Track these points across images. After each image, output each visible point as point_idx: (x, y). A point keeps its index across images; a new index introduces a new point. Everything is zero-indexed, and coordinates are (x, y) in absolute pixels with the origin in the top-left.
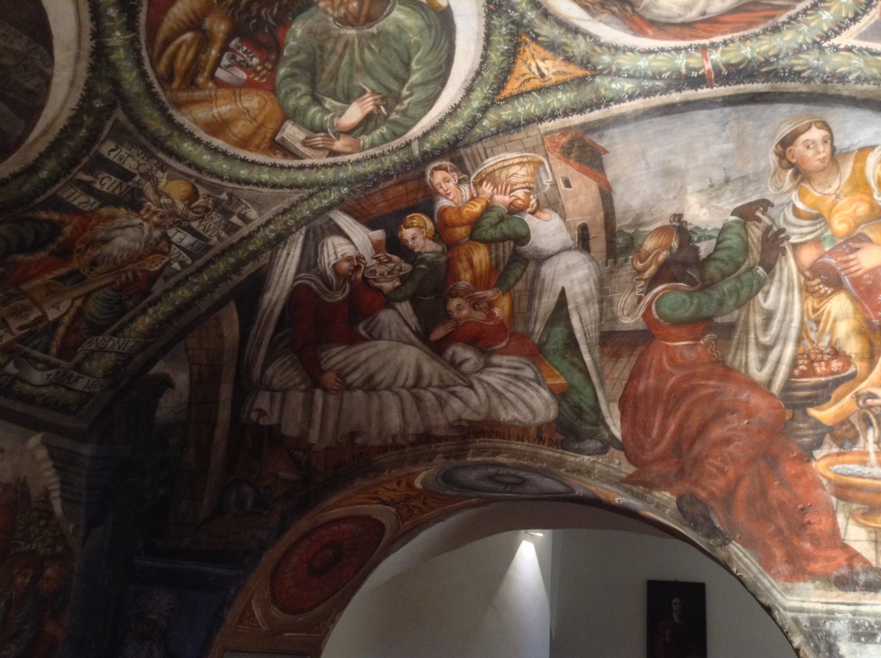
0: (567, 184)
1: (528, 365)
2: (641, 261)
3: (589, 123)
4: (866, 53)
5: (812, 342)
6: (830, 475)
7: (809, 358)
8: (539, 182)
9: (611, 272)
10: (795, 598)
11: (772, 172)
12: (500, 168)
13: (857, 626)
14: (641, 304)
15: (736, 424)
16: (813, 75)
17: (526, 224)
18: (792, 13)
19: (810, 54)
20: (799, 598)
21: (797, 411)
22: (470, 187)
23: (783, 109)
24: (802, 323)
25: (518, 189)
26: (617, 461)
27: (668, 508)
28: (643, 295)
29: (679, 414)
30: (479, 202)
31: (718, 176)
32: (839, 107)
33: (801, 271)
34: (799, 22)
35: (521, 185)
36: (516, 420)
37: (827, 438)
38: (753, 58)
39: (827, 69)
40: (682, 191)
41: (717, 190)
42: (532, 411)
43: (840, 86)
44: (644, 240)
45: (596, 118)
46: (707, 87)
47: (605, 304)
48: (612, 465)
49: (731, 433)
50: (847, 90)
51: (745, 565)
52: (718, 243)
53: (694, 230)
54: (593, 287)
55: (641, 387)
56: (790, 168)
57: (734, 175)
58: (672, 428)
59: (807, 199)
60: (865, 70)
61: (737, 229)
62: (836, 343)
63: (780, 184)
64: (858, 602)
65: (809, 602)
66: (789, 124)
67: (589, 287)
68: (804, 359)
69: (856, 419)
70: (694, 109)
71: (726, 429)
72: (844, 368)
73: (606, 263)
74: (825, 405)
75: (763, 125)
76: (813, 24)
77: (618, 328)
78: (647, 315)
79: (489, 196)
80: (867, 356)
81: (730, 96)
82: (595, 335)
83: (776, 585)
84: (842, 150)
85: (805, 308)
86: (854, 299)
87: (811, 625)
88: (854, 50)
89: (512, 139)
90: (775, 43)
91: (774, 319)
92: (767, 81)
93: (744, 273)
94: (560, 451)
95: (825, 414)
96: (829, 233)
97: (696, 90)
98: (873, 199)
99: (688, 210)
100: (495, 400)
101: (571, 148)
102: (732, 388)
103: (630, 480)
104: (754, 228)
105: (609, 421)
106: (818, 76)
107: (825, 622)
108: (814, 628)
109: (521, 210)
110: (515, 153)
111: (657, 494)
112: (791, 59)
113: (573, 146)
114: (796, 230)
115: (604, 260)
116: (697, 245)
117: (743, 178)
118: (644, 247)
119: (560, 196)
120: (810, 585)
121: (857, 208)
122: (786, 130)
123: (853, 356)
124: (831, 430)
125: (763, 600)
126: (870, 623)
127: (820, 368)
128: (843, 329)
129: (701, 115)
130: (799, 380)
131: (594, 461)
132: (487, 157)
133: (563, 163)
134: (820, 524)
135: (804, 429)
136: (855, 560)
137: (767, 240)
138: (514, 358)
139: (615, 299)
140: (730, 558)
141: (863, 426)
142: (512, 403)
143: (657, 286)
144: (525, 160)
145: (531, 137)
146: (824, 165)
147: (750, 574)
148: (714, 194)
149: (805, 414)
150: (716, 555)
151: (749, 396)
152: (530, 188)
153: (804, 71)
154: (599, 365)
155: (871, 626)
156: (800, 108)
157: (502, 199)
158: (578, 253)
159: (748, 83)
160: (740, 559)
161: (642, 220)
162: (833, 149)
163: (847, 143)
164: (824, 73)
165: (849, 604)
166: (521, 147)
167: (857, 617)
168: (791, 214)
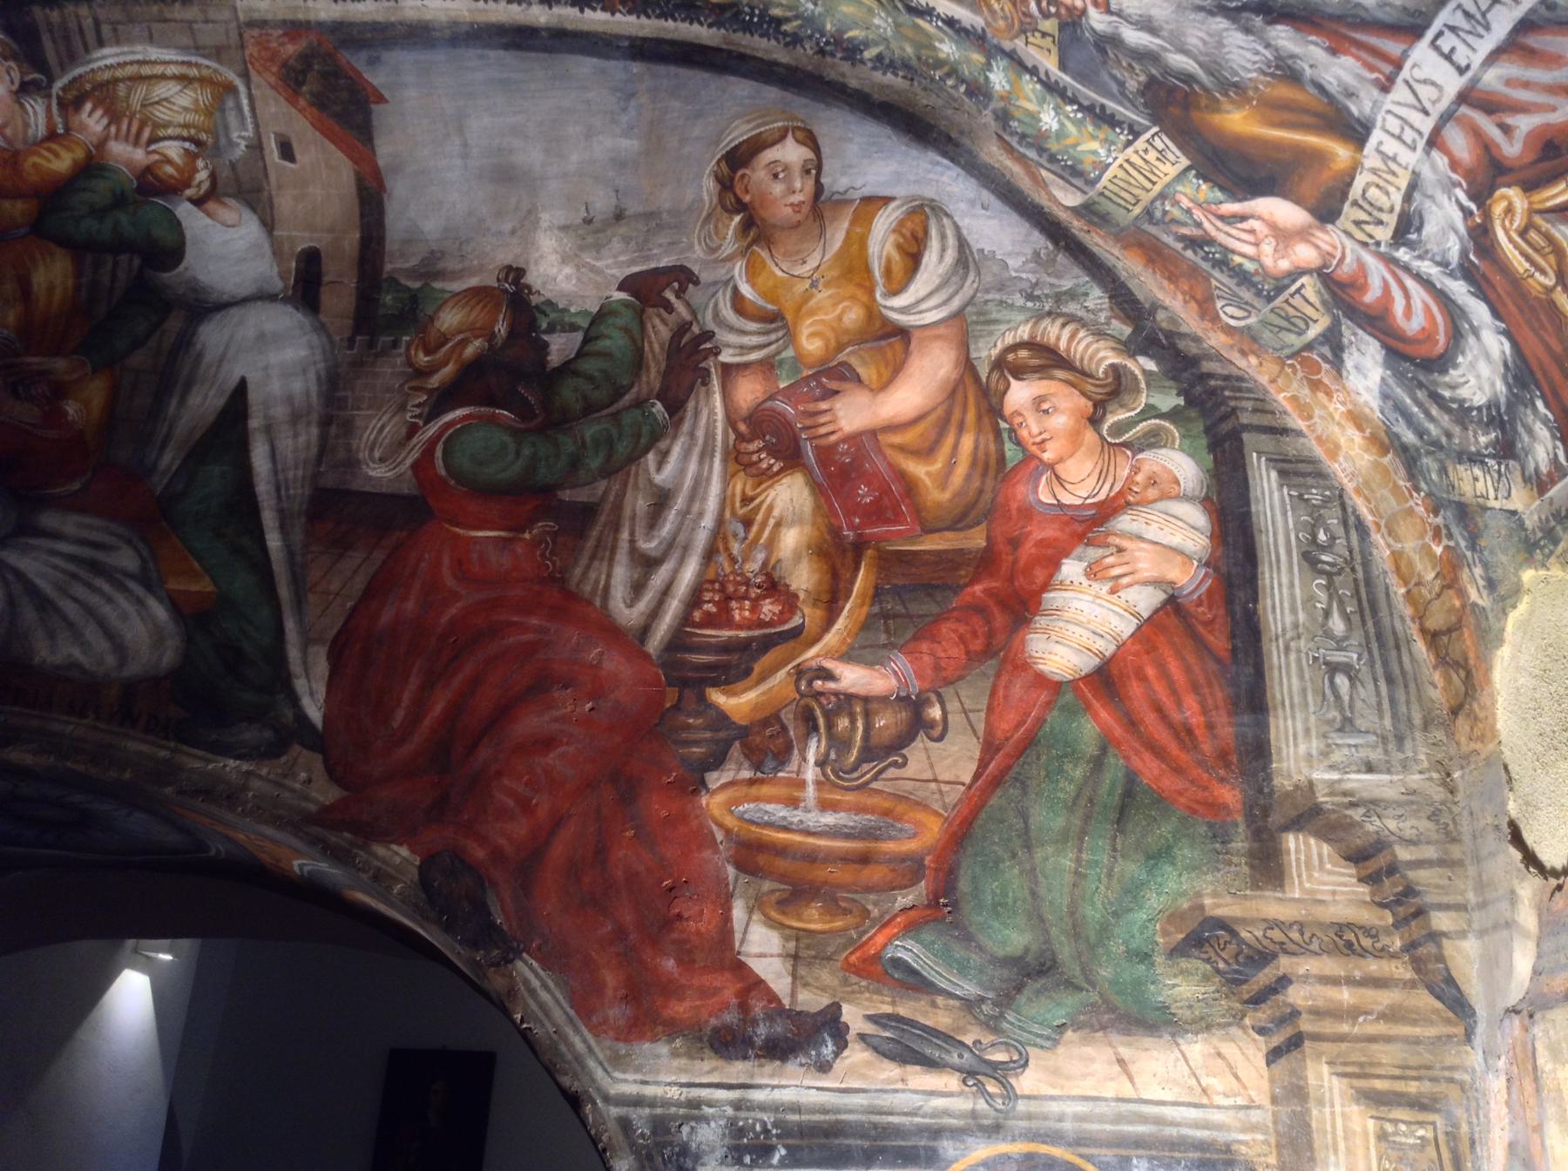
0: (287, 151)
1: (129, 542)
2: (428, 352)
3: (351, 24)
5: (733, 560)
6: (730, 821)
7: (723, 589)
8: (221, 132)
9: (357, 364)
10: (630, 1077)
11: (704, 214)
12: (130, 79)
13: (741, 1132)
14: (415, 440)
15: (569, 709)
16: (802, 33)
17: (179, 224)
20: (639, 1077)
21: (687, 692)
22: (48, 110)
23: (741, 89)
24: (720, 522)
25: (170, 138)
26: (303, 775)
27: (397, 881)
28: (421, 423)
29: (457, 681)
30: (68, 149)
31: (602, 202)
32: (839, 107)
33: (731, 421)
35: (178, 131)
36: (75, 665)
37: (736, 750)
40: (529, 220)
41: (596, 232)
42: (119, 647)
43: (845, 67)
44: (439, 308)
45: (368, 18)
46: (604, 9)
47: (333, 430)
48: (288, 782)
49: (556, 726)
51: (542, 1006)
52: (586, 341)
53: (544, 308)
54: (314, 389)
55: (386, 617)
56: (738, 212)
57: (633, 207)
58: (438, 709)
59: (760, 280)
60: (894, 45)
61: (626, 319)
62: (774, 568)
63: (717, 241)
64: (748, 1081)
65: (657, 1083)
66: (749, 122)
67: (304, 387)
68: (713, 590)
69: (791, 716)
70: (571, 51)
71: (546, 718)
72: (783, 617)
73: (351, 342)
74: (740, 685)
75: (699, 115)
77: (356, 485)
78: (422, 466)
79: (95, 140)
80: (825, 597)
81: (644, 39)
82: (299, 493)
83: (597, 1050)
84: (833, 194)
85: (729, 492)
86: (816, 488)
87: (654, 1132)
89: (168, 15)
91: (671, 508)
93: (627, 408)
94: (172, 744)
95: (738, 702)
96: (789, 353)
97: (582, 11)
98: (874, 300)
99: (536, 263)
100: (29, 614)
101: (304, 72)
102: (573, 635)
103: (326, 817)
104: (657, 321)
105: (300, 684)
106: (810, 37)
107: (680, 1126)
108: (659, 1139)
109: (173, 189)
110: (173, 52)
111: (380, 850)
113: (309, 66)
114: (733, 338)
115: (347, 334)
116: (545, 337)
117: (649, 216)
118: (437, 324)
119: (266, 175)
120: (663, 1049)
121: (843, 312)
122: (740, 132)
123: (802, 596)
124: (743, 733)
125: (566, 1081)
126: (764, 1124)
127: (740, 612)
128: (791, 539)
129: (584, 66)
130: (699, 632)
131: (249, 773)
132: (101, 44)
133: (282, 100)
134: (700, 922)
135: (697, 728)
136: (753, 993)
137: (679, 350)
138: (95, 522)
139: (359, 423)
140: (512, 992)
141: (802, 730)
142: (71, 625)
143: (453, 408)
144: (194, 72)
145: (213, 22)
146: (799, 217)
147: (548, 1025)
148: (590, 239)
149: (702, 698)
150: (485, 985)
151: (601, 654)
152: (198, 143)
153: (787, 20)
154: (299, 559)
155: (766, 1131)
156: (772, 93)
157: (126, 154)
158: (290, 309)
159: (683, 20)
160: (532, 992)
161: (440, 266)
162: (819, 188)
163: (842, 183)
164: (823, 35)
165: (730, 1087)
166: (186, 41)
167: (743, 1114)
168: (729, 305)
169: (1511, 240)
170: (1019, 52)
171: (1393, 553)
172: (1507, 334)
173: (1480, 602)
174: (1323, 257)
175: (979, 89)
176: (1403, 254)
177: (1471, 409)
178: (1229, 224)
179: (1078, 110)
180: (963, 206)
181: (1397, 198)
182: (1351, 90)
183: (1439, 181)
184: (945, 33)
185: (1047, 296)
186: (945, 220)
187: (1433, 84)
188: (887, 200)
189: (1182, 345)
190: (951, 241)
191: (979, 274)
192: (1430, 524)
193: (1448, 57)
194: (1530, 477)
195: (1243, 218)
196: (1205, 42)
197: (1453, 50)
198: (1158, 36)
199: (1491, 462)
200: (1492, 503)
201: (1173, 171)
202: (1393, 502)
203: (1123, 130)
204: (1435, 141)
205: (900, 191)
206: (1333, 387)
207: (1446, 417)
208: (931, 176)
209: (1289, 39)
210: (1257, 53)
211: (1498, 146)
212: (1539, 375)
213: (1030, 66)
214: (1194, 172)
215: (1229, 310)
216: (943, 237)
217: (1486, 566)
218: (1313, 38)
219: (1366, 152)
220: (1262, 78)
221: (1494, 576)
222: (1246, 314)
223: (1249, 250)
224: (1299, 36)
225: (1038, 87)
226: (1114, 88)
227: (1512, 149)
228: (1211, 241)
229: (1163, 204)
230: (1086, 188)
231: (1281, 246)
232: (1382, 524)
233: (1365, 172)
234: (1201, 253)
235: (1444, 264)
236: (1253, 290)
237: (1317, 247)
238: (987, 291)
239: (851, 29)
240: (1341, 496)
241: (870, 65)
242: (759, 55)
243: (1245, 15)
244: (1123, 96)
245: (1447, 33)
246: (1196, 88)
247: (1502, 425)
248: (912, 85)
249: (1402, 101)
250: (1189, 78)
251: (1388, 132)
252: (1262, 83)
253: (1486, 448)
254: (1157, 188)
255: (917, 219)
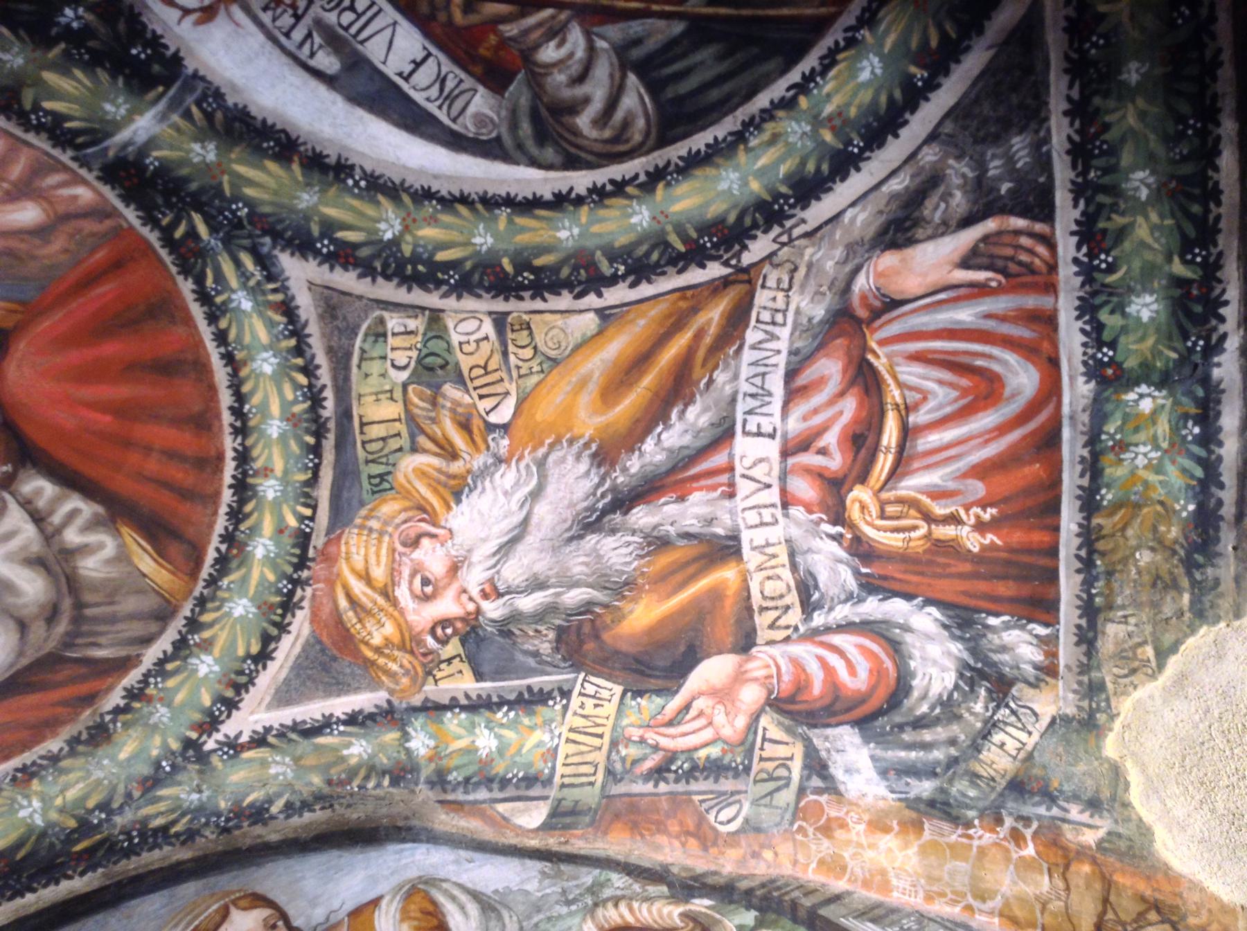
4: (294, 736)
16: (195, 825)
18: (132, 678)
19: (180, 784)
32: (272, 861)
34: (149, 700)
38: (50, 825)
39: (223, 805)
43: (258, 830)
50: (276, 832)
76: (179, 697)
88: (271, 739)
90: (99, 774)
92: (93, 868)
106: (207, 824)
112: (139, 808)
153: (174, 823)
156: (189, 890)
159: (45, 886)
164: (219, 815)
169: (878, 529)
170: (432, 697)
171: (1001, 915)
172: (929, 602)
173: (1101, 833)
174: (763, 685)
175: (404, 770)
176: (818, 619)
177: (950, 695)
178: (679, 723)
179: (509, 710)
180: (452, 868)
181: (786, 574)
182: (709, 517)
183: (807, 531)
184: (350, 734)
185: (581, 895)
186: (445, 885)
187: (761, 460)
188: (375, 902)
189: (710, 880)
190: (463, 898)
191: (509, 909)
192: (1005, 839)
193: (759, 434)
194: (1038, 679)
195: (687, 707)
196: (586, 564)
197: (759, 426)
198: (548, 587)
199: (1003, 713)
200: (1031, 741)
201: (610, 709)
202: (961, 865)
203: (554, 698)
204: (787, 501)
205: (383, 888)
206: (842, 814)
207: (939, 729)
208: (404, 862)
209: (647, 514)
210: (629, 544)
211: (826, 468)
212: (972, 603)
213: (446, 701)
214: (629, 694)
215: (724, 816)
216: (453, 898)
217: (1075, 798)
218: (663, 500)
219: (745, 557)
220: (642, 562)
221: (1089, 794)
222: (738, 806)
223: (707, 734)
224: (651, 507)
225: (463, 716)
226: (531, 662)
227: (835, 463)
228: (672, 756)
229: (618, 752)
230: (545, 792)
231: (729, 706)
232: (971, 900)
233: (754, 575)
234: (671, 776)
235: (850, 597)
236: (730, 774)
237: (756, 680)
238: (529, 917)
239: (248, 795)
240: (922, 915)
241: (282, 816)
242: (156, 866)
243: (606, 519)
244: (543, 666)
245: (749, 417)
246: (597, 610)
247: (982, 675)
248: (334, 811)
249: (748, 493)
250: (587, 607)
251: (751, 527)
252: (644, 566)
253: (987, 709)
254: (607, 739)
255: (417, 898)
